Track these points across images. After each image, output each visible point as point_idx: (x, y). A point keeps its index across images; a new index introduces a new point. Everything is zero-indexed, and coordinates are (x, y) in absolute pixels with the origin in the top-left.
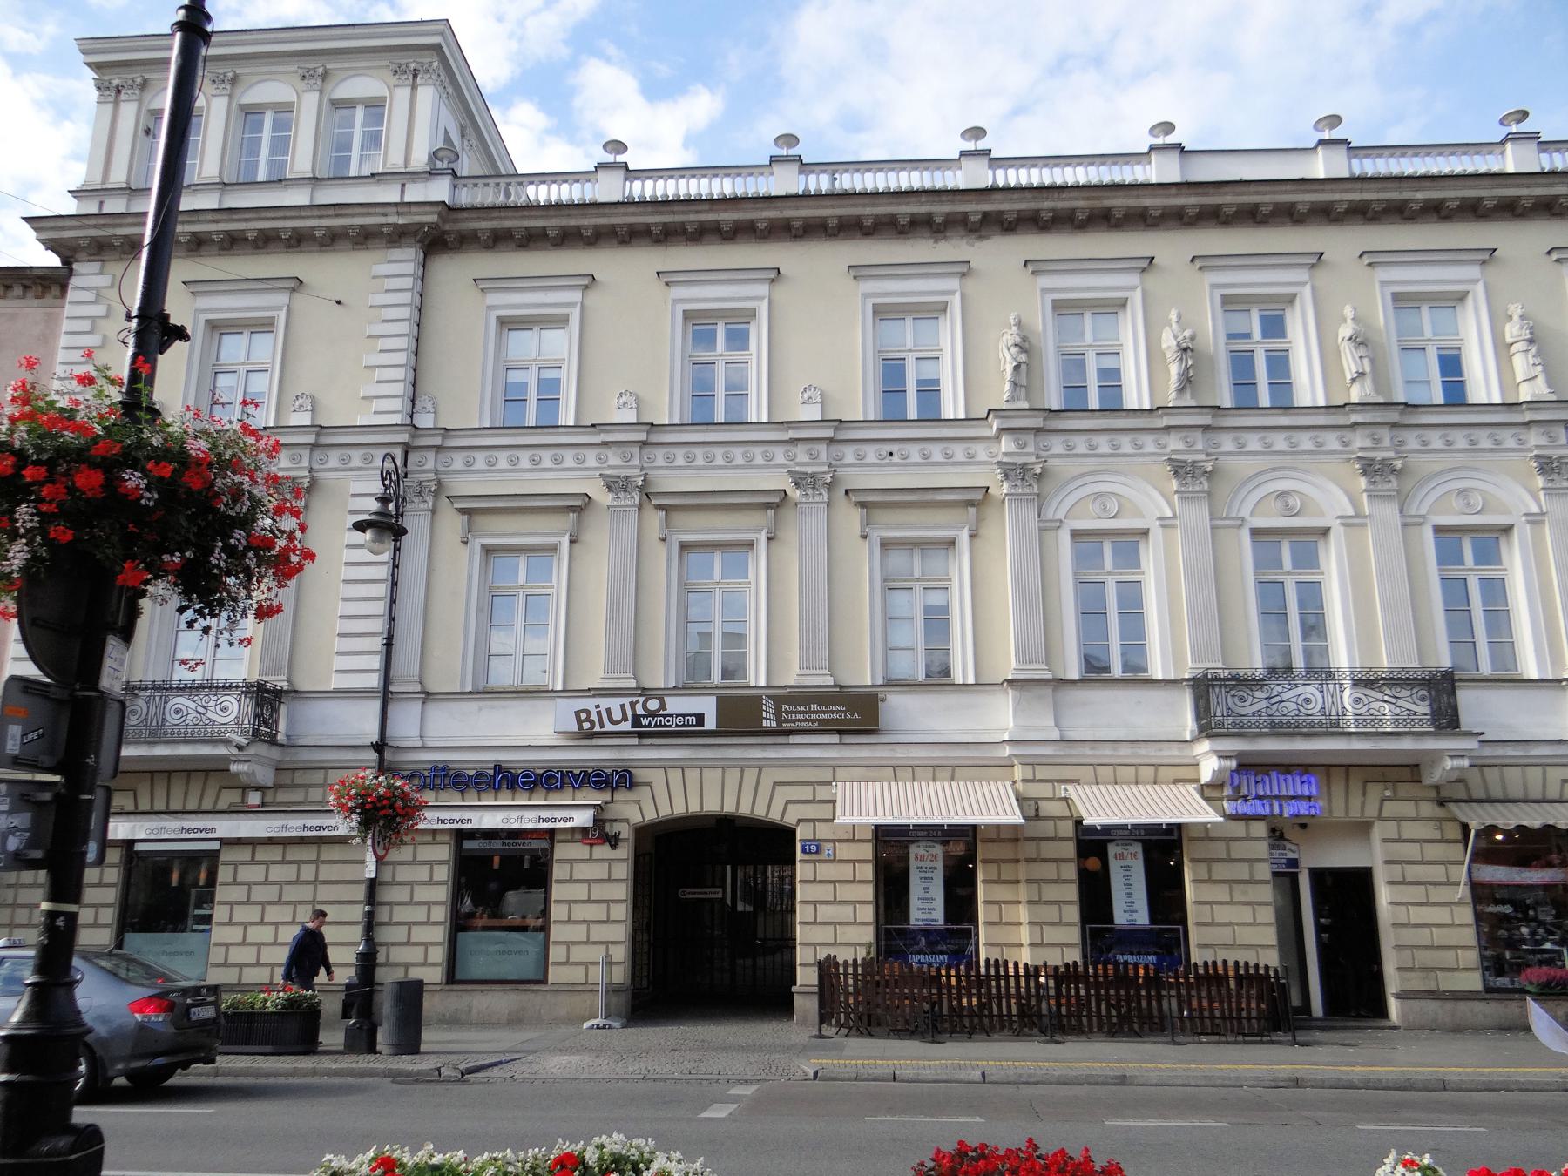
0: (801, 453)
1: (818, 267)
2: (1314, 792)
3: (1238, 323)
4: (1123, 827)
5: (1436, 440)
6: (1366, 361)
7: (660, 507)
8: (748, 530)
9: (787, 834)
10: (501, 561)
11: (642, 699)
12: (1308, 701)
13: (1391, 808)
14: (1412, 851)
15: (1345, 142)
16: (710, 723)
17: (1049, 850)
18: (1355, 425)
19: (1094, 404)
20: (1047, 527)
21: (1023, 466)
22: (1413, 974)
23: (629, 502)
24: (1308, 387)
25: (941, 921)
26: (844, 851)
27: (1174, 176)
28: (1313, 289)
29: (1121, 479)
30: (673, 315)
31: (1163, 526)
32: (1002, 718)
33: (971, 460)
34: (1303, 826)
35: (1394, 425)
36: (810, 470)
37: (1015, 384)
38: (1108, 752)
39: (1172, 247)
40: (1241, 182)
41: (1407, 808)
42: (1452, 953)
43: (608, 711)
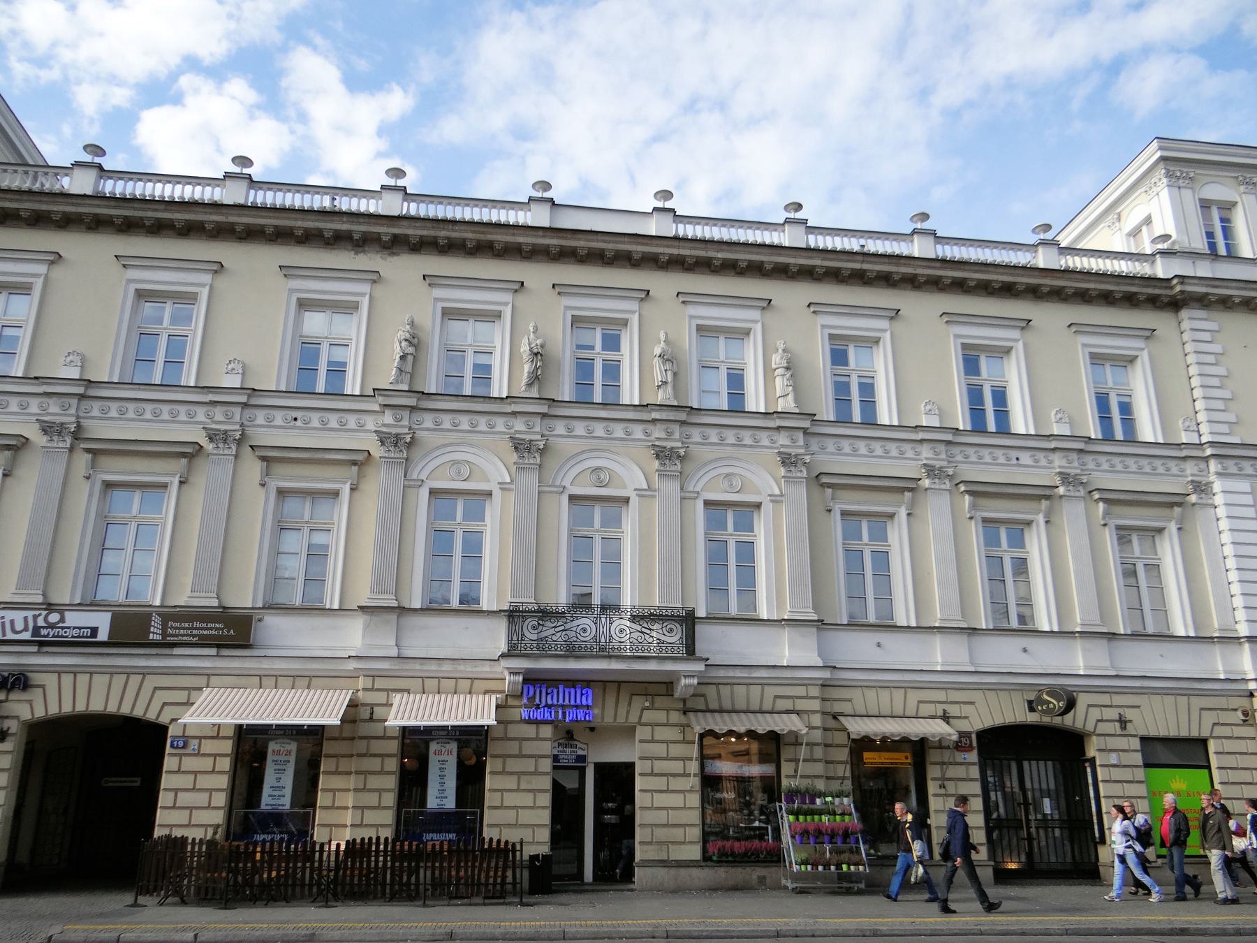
0: (219, 413)
1: (255, 264)
2: (590, 702)
3: (585, 337)
4: (444, 728)
5: (713, 436)
6: (669, 373)
7: (88, 451)
8: (167, 474)
9: (161, 730)
10: (118, 495)
11: (44, 613)
12: (534, 627)
13: (649, 716)
14: (660, 750)
15: (673, 211)
16: (103, 636)
17: (377, 747)
18: (654, 421)
19: (598, 398)
20: (410, 486)
21: (397, 435)
22: (650, 847)
23: (61, 445)
24: (630, 393)
25: (288, 807)
26: (208, 747)
27: (545, 222)
28: (1025, 345)
29: (473, 450)
30: (126, 291)
31: (772, 501)
32: (352, 637)
33: (361, 427)
34: (592, 729)
35: (683, 423)
36: (223, 427)
37: (400, 370)
38: (418, 667)
39: (539, 276)
40: (591, 232)
41: (660, 716)
42: (682, 830)
43: (12, 622)
